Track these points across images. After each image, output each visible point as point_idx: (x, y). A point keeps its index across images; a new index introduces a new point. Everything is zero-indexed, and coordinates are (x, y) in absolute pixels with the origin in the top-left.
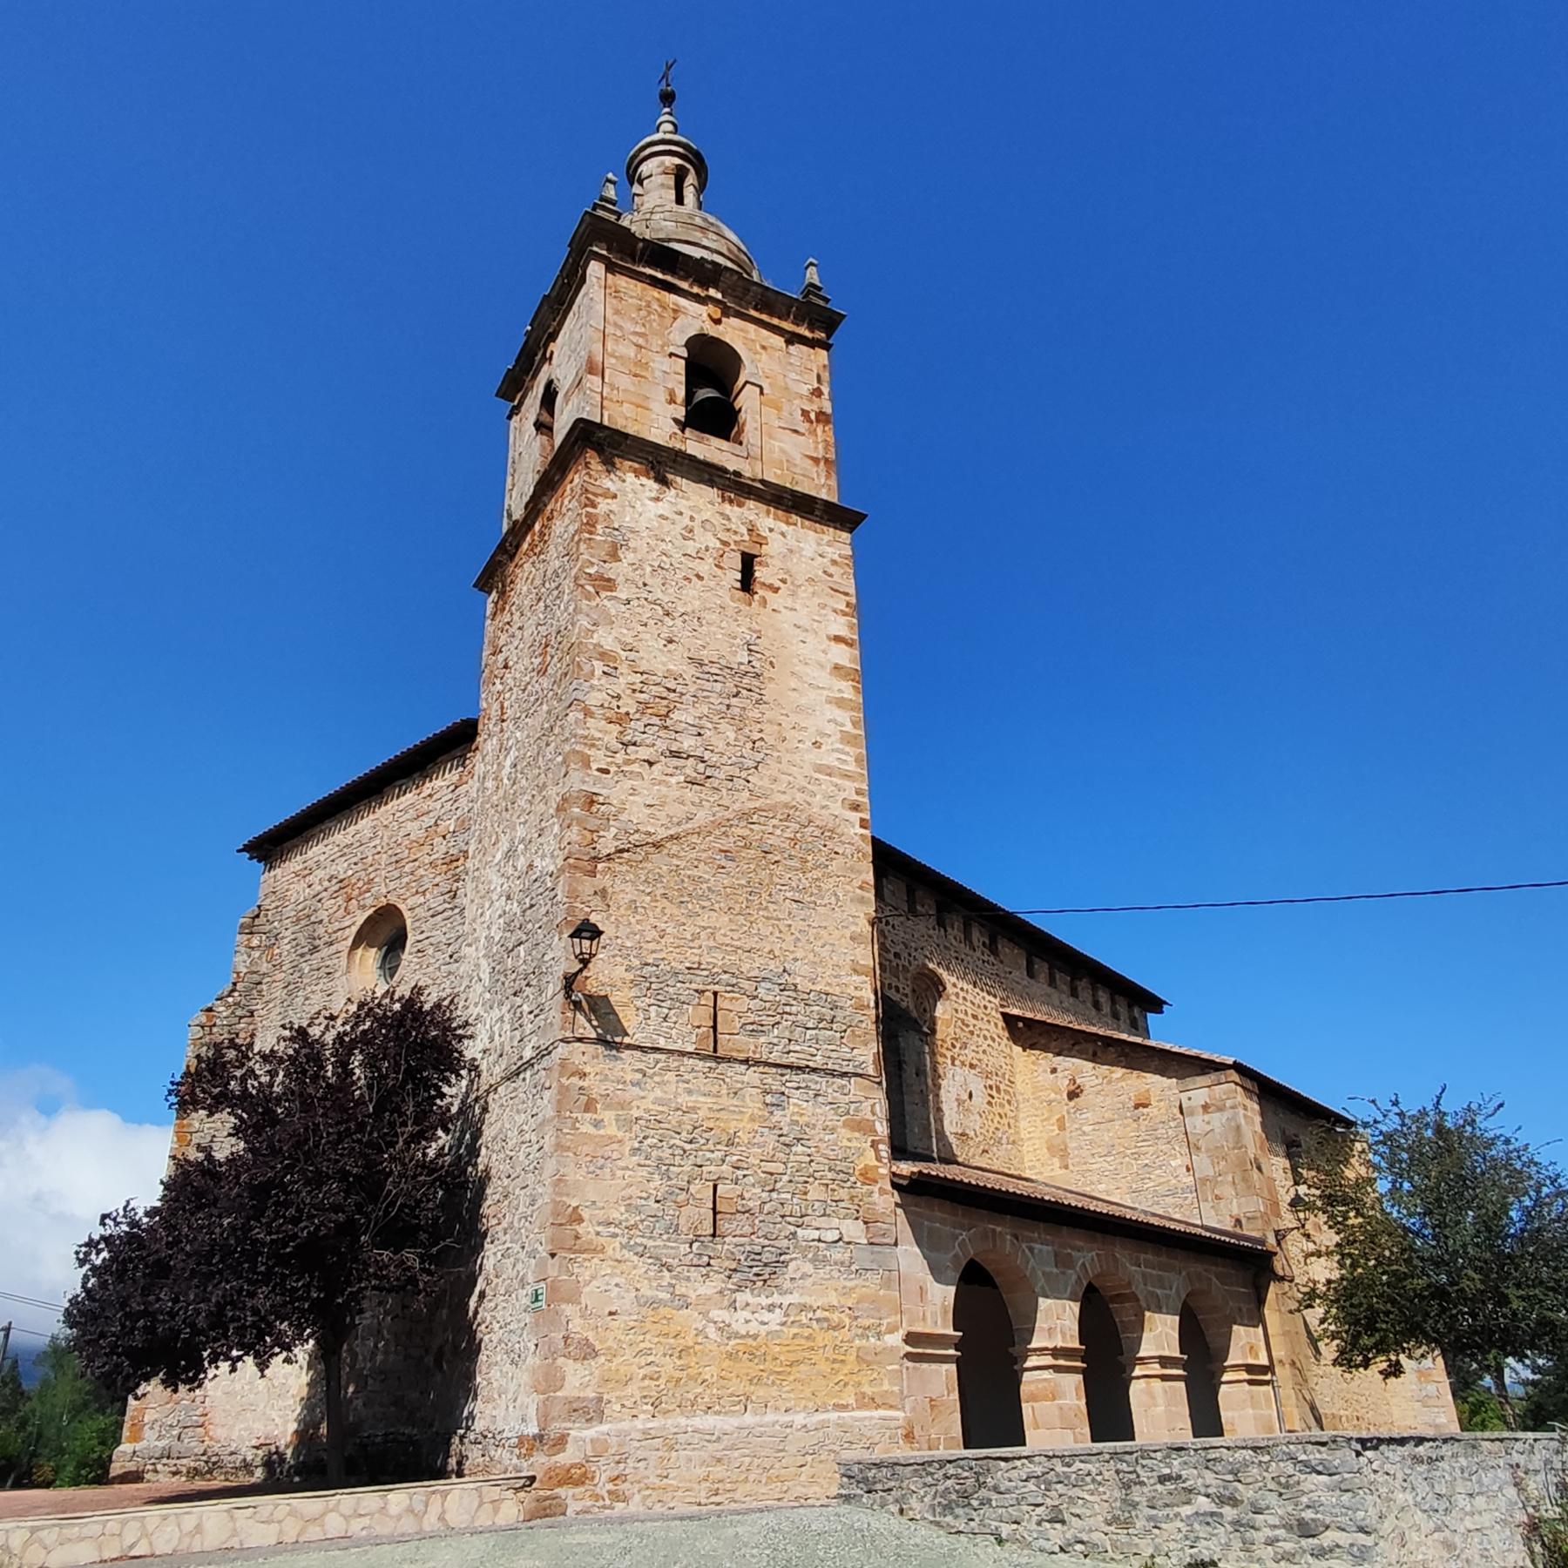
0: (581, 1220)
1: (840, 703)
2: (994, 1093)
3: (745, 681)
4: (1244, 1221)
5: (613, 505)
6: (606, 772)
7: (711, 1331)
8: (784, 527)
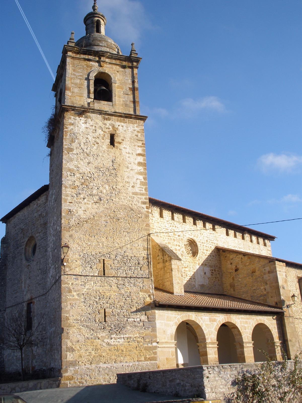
0: (69, 319)
1: (140, 173)
2: (214, 272)
3: (114, 170)
4: (278, 303)
5: (72, 127)
6: (72, 203)
7: (104, 344)
8: (123, 124)
